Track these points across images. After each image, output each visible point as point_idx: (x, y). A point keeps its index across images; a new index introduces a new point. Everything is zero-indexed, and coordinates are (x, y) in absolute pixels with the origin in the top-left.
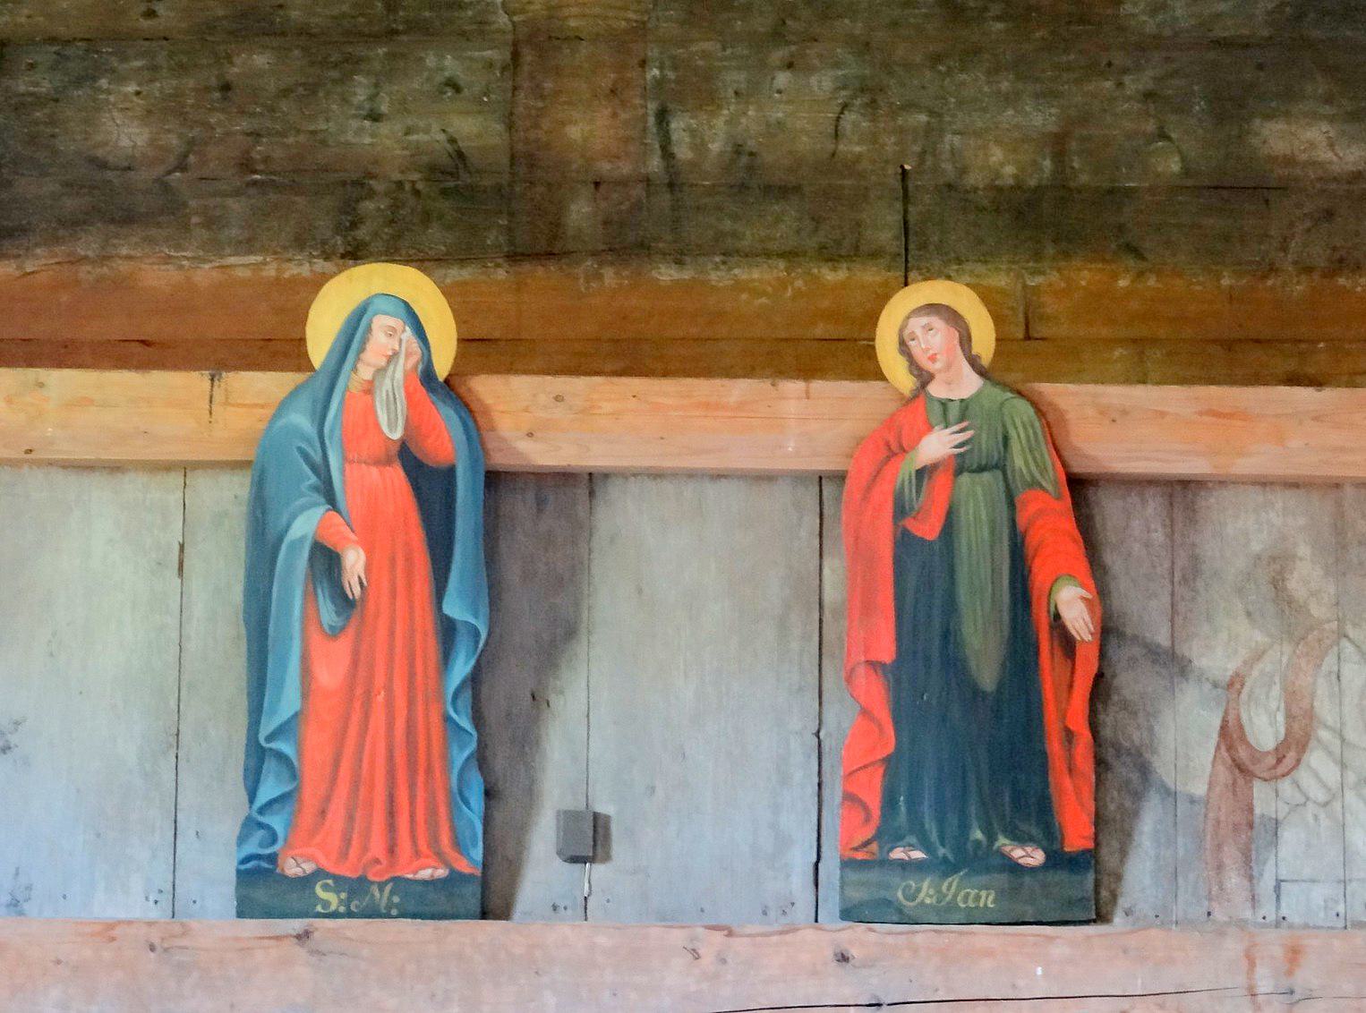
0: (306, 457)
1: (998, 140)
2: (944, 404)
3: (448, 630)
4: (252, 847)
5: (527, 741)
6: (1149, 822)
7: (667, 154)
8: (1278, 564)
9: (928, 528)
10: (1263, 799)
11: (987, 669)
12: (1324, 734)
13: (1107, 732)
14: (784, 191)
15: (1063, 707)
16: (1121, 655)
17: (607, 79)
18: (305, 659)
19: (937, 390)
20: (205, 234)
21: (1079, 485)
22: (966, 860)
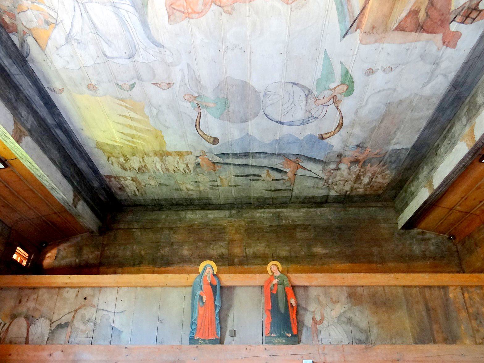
0: (199, 284)
1: (284, 252)
2: (276, 276)
3: (216, 306)
4: (191, 335)
5: (226, 321)
6: (304, 330)
7: (246, 253)
8: (318, 297)
9: (275, 292)
10: (319, 327)
11: (282, 310)
12: (325, 318)
13: (298, 318)
14: (259, 257)
15: (293, 316)
16: (299, 308)
17: (239, 245)
18: (198, 310)
19: (275, 275)
20: (194, 264)
21: (293, 287)
22: (281, 336)
